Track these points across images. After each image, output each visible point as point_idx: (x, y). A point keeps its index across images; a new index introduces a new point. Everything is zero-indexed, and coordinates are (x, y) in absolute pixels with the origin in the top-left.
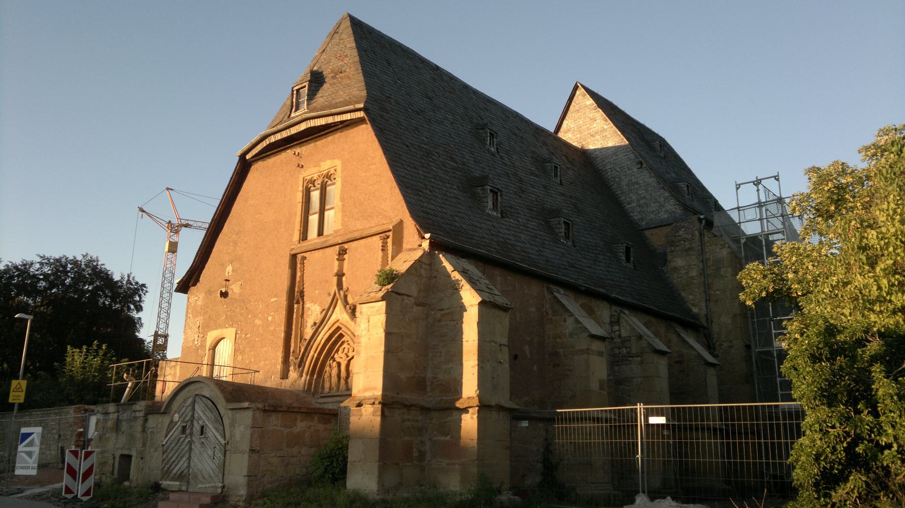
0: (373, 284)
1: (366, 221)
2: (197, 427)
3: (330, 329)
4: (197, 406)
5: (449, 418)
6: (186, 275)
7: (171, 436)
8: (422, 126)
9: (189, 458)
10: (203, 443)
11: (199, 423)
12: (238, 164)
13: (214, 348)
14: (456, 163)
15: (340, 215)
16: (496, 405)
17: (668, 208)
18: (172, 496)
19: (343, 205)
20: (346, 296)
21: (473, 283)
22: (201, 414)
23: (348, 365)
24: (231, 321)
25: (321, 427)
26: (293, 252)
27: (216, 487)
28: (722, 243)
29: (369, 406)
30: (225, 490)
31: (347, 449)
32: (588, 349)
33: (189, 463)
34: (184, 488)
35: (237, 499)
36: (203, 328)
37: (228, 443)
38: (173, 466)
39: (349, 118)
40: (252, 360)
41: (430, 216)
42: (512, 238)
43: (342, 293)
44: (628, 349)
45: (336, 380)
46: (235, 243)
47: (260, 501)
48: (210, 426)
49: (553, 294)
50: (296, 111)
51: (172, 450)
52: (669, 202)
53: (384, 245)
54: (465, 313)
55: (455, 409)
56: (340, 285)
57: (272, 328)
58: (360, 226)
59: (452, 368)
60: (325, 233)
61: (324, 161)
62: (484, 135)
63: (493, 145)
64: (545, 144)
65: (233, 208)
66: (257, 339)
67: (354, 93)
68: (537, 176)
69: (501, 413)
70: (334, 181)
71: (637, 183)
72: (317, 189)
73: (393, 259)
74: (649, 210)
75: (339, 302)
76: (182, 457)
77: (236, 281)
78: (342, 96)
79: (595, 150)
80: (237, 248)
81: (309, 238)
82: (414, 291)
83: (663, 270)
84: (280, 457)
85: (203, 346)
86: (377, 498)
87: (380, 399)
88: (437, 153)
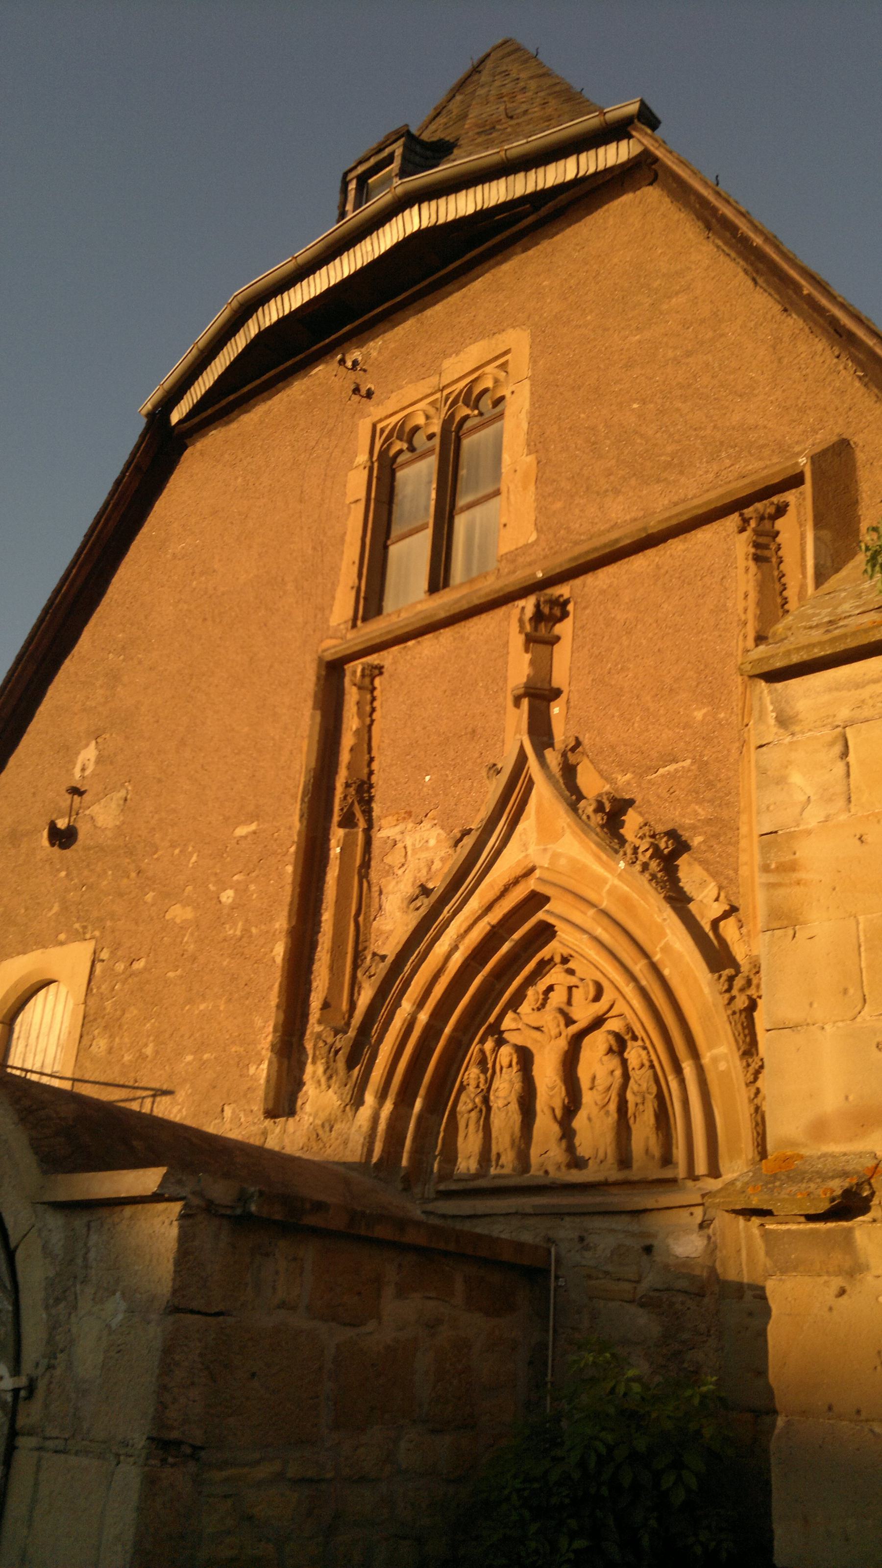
1: (658, 488)
3: (489, 908)
12: (143, 436)
20: (569, 771)
37: (31, 1388)
39: (570, 175)
40: (149, 1050)
43: (552, 757)
45: (516, 1118)
50: (357, 205)
53: (762, 540)
57: (234, 931)
66: (171, 974)
77: (106, 792)
84: (303, 1480)
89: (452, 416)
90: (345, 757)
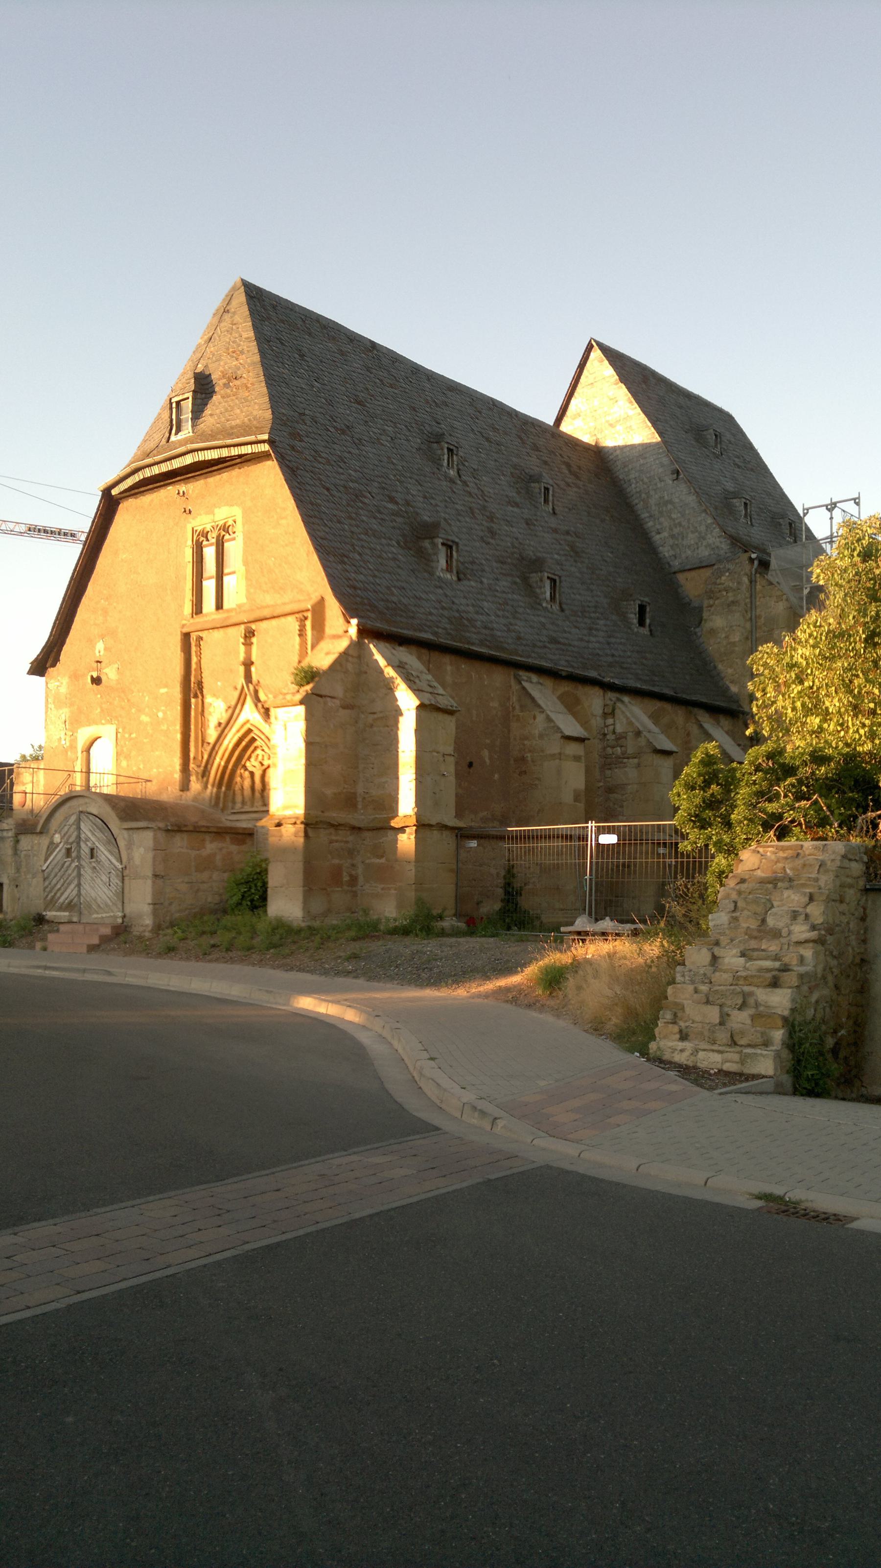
0: (290, 684)
2: (85, 849)
3: (238, 731)
4: (82, 826)
5: (384, 839)
6: (41, 653)
7: (53, 859)
8: (350, 452)
9: (79, 885)
10: (94, 868)
11: (87, 845)
12: (101, 501)
13: (88, 750)
14: (397, 503)
15: (243, 583)
16: (438, 824)
17: (710, 541)
18: (62, 928)
19: (247, 571)
20: (256, 692)
21: (410, 680)
22: (90, 835)
23: (263, 776)
24: (108, 716)
25: (234, 848)
26: (185, 630)
27: (116, 917)
28: (779, 593)
29: (291, 826)
30: (125, 920)
31: (267, 874)
32: (560, 754)
33: (79, 891)
34: (75, 919)
35: (141, 929)
36: (71, 723)
37: (126, 867)
38: (58, 895)
39: (250, 452)
40: (141, 766)
41: (359, 592)
42: (471, 609)
44: (623, 749)
46: (105, 612)
47: (170, 931)
48: (102, 848)
49: (521, 683)
50: (176, 434)
51: (56, 876)
52: (712, 531)
54: (401, 719)
55: (390, 829)
56: (248, 677)
57: (164, 727)
58: (269, 600)
59: (386, 782)
60: (226, 605)
61: (220, 507)
62: (439, 452)
63: (453, 467)
64: (536, 448)
65: (98, 562)
67: (255, 413)
68: (517, 505)
69: (444, 832)
70: (233, 536)
71: (670, 502)
72: (211, 545)
73: (313, 647)
74: (685, 543)
75: (249, 700)
76: (69, 884)
77: (110, 664)
78: (239, 417)
79: (615, 448)
80: (108, 618)
81: (205, 610)
82: (339, 691)
83: (696, 633)
84: (187, 883)
85: (73, 747)
86: (303, 925)
87: (302, 819)
88: (370, 493)
89: (220, 534)
90: (193, 673)
